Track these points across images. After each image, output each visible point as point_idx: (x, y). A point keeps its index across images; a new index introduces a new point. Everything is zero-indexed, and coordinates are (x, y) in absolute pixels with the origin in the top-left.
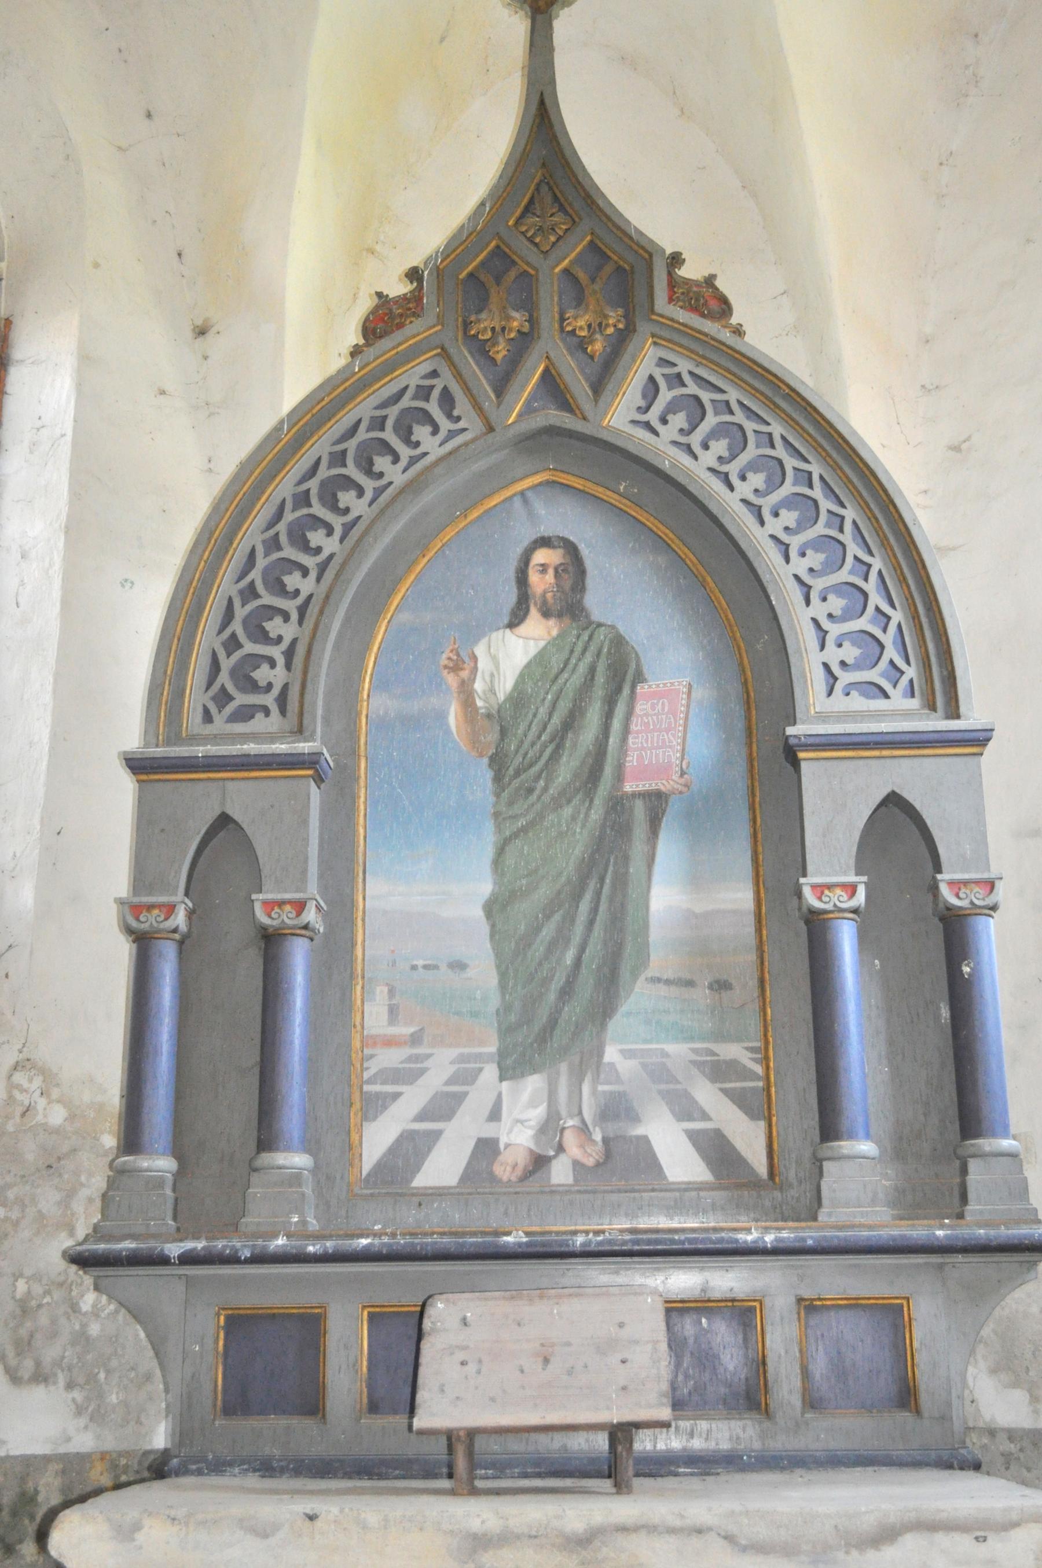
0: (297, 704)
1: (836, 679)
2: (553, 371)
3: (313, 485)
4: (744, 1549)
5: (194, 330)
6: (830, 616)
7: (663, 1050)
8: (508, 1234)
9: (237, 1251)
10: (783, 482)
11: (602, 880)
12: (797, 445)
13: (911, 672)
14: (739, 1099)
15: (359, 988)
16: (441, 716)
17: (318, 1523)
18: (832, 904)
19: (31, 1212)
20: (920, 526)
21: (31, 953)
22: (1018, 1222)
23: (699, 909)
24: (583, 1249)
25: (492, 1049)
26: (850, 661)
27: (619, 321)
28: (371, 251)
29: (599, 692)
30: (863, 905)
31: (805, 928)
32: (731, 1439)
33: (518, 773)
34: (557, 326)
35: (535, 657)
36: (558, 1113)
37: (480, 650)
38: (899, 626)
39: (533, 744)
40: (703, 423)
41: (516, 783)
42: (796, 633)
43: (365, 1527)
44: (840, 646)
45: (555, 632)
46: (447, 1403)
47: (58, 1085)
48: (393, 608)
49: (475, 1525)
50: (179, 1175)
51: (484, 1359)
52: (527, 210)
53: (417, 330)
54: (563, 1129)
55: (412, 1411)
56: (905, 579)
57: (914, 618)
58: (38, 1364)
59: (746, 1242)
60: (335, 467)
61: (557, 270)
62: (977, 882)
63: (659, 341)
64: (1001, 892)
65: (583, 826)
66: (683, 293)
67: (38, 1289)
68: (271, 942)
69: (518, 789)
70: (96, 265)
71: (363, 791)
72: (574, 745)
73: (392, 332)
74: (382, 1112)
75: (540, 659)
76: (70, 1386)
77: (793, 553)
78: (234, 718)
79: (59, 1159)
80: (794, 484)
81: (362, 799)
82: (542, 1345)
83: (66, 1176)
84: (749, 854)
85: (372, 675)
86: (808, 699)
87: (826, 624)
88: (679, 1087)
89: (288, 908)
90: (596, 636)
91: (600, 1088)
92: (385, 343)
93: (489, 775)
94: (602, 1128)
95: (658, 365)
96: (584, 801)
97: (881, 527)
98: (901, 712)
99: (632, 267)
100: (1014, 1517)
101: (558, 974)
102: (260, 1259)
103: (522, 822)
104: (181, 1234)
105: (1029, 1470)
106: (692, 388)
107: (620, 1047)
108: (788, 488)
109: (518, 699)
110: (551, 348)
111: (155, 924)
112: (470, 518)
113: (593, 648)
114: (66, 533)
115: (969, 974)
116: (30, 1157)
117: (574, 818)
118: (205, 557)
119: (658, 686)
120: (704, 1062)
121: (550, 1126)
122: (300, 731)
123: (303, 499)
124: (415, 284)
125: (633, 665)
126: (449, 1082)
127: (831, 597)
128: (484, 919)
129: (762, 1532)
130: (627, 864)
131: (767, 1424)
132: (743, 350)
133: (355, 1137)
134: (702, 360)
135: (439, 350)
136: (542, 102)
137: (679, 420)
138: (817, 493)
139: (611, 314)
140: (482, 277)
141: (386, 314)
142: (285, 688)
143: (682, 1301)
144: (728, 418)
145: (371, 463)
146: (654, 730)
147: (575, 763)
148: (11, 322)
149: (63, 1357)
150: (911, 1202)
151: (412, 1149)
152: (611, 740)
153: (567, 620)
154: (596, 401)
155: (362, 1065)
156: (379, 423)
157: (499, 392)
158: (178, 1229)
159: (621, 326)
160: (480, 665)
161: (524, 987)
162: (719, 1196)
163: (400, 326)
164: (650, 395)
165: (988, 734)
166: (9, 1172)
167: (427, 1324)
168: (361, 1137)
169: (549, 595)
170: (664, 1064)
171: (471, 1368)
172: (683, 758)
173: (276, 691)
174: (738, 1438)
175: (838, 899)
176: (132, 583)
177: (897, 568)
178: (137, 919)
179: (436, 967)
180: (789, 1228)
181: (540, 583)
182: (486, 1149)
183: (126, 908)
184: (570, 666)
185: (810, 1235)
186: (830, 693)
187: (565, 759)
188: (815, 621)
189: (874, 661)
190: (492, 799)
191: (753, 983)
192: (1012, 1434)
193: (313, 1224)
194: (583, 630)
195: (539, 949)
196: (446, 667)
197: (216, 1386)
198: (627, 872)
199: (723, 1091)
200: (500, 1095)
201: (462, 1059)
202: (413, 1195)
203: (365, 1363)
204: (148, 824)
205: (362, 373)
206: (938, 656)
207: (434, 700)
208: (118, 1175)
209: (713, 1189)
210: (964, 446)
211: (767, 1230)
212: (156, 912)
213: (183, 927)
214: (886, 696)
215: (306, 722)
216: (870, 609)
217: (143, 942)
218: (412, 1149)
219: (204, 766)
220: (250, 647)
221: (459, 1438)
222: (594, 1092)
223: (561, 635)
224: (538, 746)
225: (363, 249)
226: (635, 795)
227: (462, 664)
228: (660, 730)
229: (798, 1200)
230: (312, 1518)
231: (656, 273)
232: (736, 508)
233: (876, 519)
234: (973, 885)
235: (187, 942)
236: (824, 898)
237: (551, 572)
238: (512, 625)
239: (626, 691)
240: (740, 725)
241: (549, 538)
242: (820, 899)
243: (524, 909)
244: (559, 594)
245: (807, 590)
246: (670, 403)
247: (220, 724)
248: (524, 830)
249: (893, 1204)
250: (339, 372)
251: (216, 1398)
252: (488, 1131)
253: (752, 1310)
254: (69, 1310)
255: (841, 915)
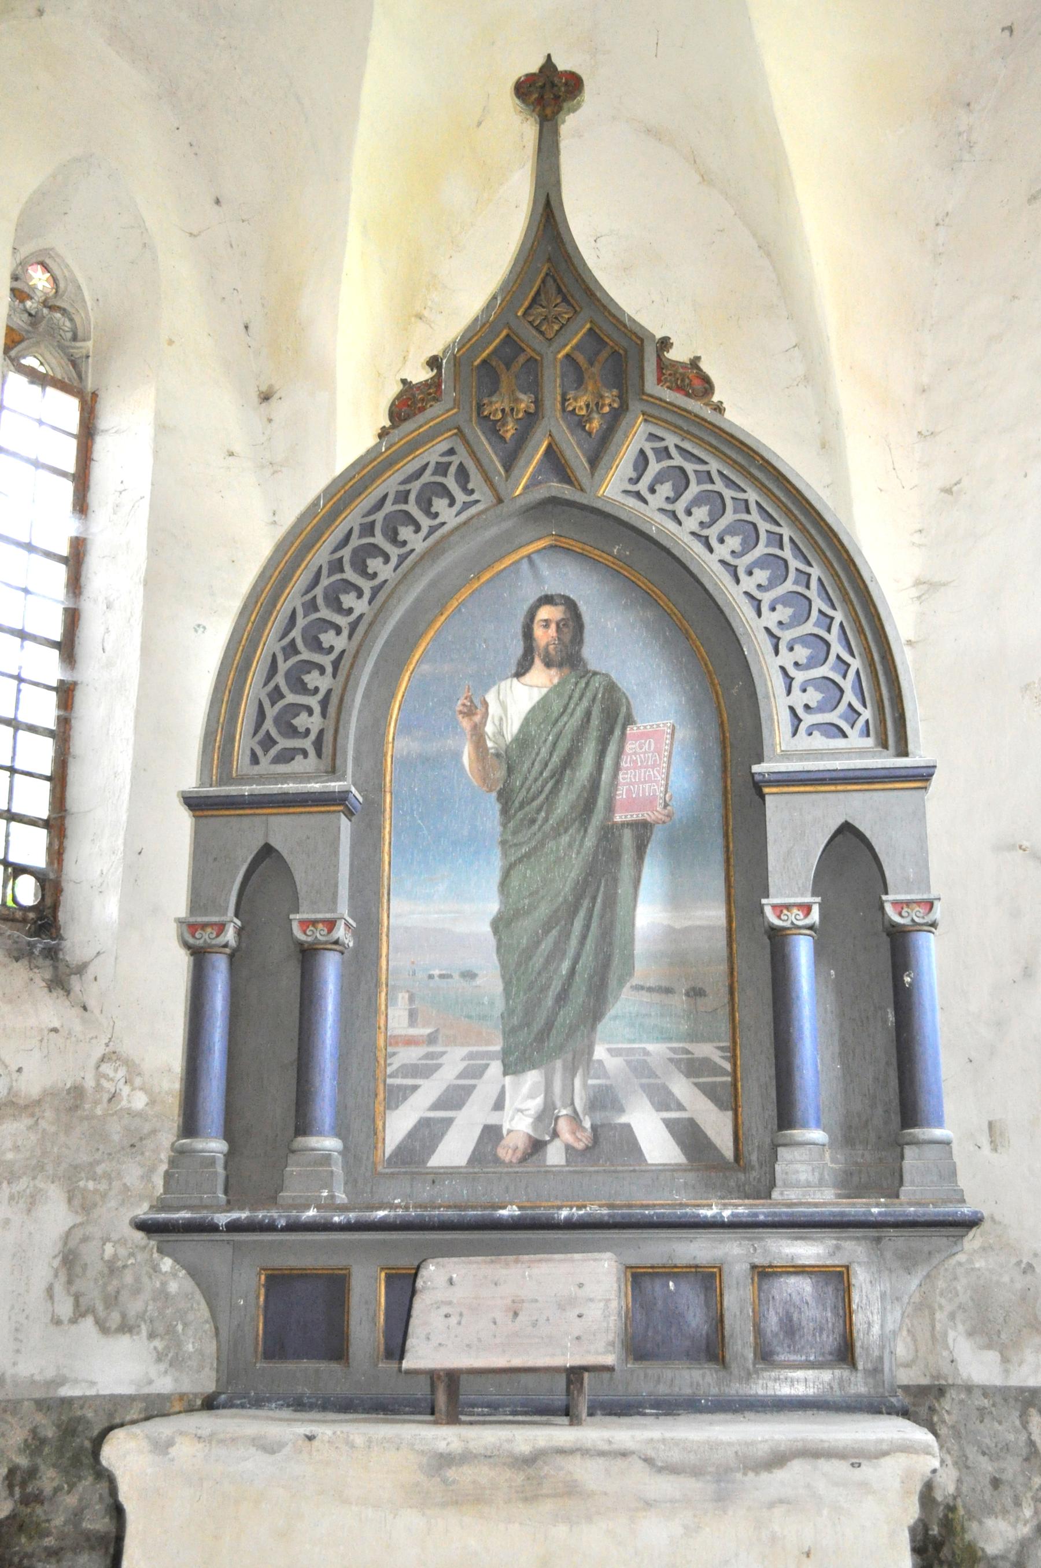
0: (331, 746)
1: (800, 720)
2: (555, 447)
3: (346, 553)
4: (660, 1470)
5: (259, 395)
6: (796, 664)
7: (644, 1049)
8: (504, 1208)
9: (274, 1221)
10: (757, 544)
11: (594, 899)
12: (770, 510)
13: (867, 714)
14: (710, 1092)
15: (383, 994)
16: (457, 755)
17: (316, 1443)
18: (789, 922)
19: (117, 1184)
20: (877, 583)
21: (116, 958)
22: (945, 1202)
23: (677, 926)
24: (731, 1219)
25: (497, 1048)
26: (813, 704)
27: (614, 401)
28: (420, 317)
29: (593, 734)
30: (817, 922)
31: (768, 941)
32: (691, 1385)
33: (522, 806)
34: (559, 406)
35: (538, 702)
36: (553, 1104)
37: (491, 697)
38: (858, 672)
39: (536, 780)
40: (687, 492)
41: (520, 815)
42: (766, 680)
43: (353, 1446)
44: (804, 691)
45: (556, 681)
46: (430, 1350)
47: (139, 1074)
48: (414, 661)
49: (442, 1446)
50: (229, 1156)
51: (467, 1313)
52: (534, 301)
53: (436, 413)
54: (557, 1118)
55: (402, 1357)
56: (863, 630)
57: (870, 665)
58: (124, 1316)
59: (706, 1217)
60: (365, 536)
61: (560, 356)
62: (918, 903)
63: (650, 419)
64: (939, 911)
65: (578, 853)
66: (670, 375)
67: (123, 1252)
68: (308, 956)
69: (522, 820)
70: (171, 342)
71: (388, 822)
72: (571, 781)
73: (415, 415)
74: (402, 1102)
75: (543, 704)
76: (152, 1336)
77: (765, 608)
78: (278, 759)
79: (141, 1139)
80: (767, 546)
81: (387, 830)
82: (513, 1302)
83: (147, 1154)
84: (723, 875)
85: (396, 720)
86: (774, 738)
87: (792, 671)
88: (658, 1081)
89: (320, 926)
90: (592, 682)
91: (590, 1082)
92: (408, 426)
93: (498, 807)
94: (591, 1117)
95: (647, 440)
96: (579, 830)
97: (842, 583)
98: (858, 750)
99: (626, 351)
100: (885, 1447)
101: (554, 983)
102: (294, 1227)
103: (524, 849)
104: (230, 1206)
105: (1000, 1423)
106: (678, 460)
107: (607, 1046)
108: (761, 550)
109: (524, 740)
110: (554, 426)
111: (209, 941)
112: (482, 581)
113: (589, 694)
114: (145, 585)
115: (910, 984)
116: (116, 1138)
117: (570, 845)
118: (253, 618)
119: (645, 727)
120: (681, 1060)
121: (546, 1116)
122: (333, 771)
123: (337, 566)
124: (435, 371)
125: (624, 709)
126: (460, 1076)
127: (797, 647)
128: (491, 934)
129: (675, 1456)
130: (616, 886)
131: (722, 1374)
132: (723, 425)
133: (380, 1124)
134: (686, 434)
135: (455, 431)
136: (548, 204)
137: (665, 489)
138: (787, 553)
139: (607, 395)
140: (494, 364)
141: (409, 399)
142: (321, 732)
143: (652, 1267)
144: (709, 487)
145: (396, 533)
146: (640, 767)
147: (572, 796)
148: (97, 396)
149: (146, 1311)
150: (852, 1184)
151: (427, 1134)
152: (603, 776)
153: (566, 670)
154: (592, 474)
155: (385, 1061)
156: (403, 497)
157: (508, 467)
158: (228, 1202)
159: (616, 405)
160: (491, 710)
161: (525, 994)
162: (691, 1177)
163: (422, 410)
164: (640, 469)
165: (930, 771)
166: (98, 1150)
167: (419, 1283)
168: (384, 1124)
169: (551, 647)
170: (645, 1061)
171: (453, 1320)
172: (666, 792)
173: (313, 736)
174: (698, 1384)
175: (796, 917)
176: (204, 628)
177: (856, 620)
178: (193, 936)
179: (450, 976)
180: (745, 1205)
181: (544, 636)
182: (491, 1134)
183: (185, 928)
184: (569, 711)
185: (762, 1211)
186: (795, 733)
187: (563, 793)
188: (782, 668)
189: (835, 704)
190: (499, 829)
191: (724, 991)
192: (986, 1391)
193: (341, 1197)
194: (581, 677)
195: (538, 961)
196: (461, 712)
197: (258, 1335)
198: (616, 893)
199: (696, 1084)
200: (503, 1087)
201: (471, 1056)
202: (427, 1174)
203: (382, 1317)
204: (204, 856)
205: (389, 452)
206: (891, 699)
207: (450, 742)
208: (179, 1155)
209: (685, 1171)
210: (955, 489)
211: (725, 1206)
212: (209, 930)
213: (233, 943)
214: (845, 736)
215: (338, 762)
216: (832, 657)
217: (199, 955)
218: (427, 1134)
219: (249, 803)
220: (291, 698)
221: (439, 1377)
222: (585, 1085)
223: (563, 682)
224: (539, 783)
225: (412, 314)
226: (624, 825)
227: (475, 709)
228: (647, 767)
229: (759, 1180)
230: (310, 1438)
231: (647, 356)
232: (714, 568)
233: (839, 577)
234: (915, 905)
235: (237, 954)
236: (783, 917)
237: (553, 626)
238: (518, 675)
239: (617, 732)
240: (717, 762)
241: (552, 596)
242: (779, 917)
243: (527, 925)
244: (560, 647)
245: (776, 640)
246: (659, 473)
247: (266, 765)
248: (527, 856)
249: (835, 1186)
250: (368, 452)
251: (257, 1344)
252: (493, 1119)
253: (713, 1275)
254: (151, 1271)
255: (798, 931)
